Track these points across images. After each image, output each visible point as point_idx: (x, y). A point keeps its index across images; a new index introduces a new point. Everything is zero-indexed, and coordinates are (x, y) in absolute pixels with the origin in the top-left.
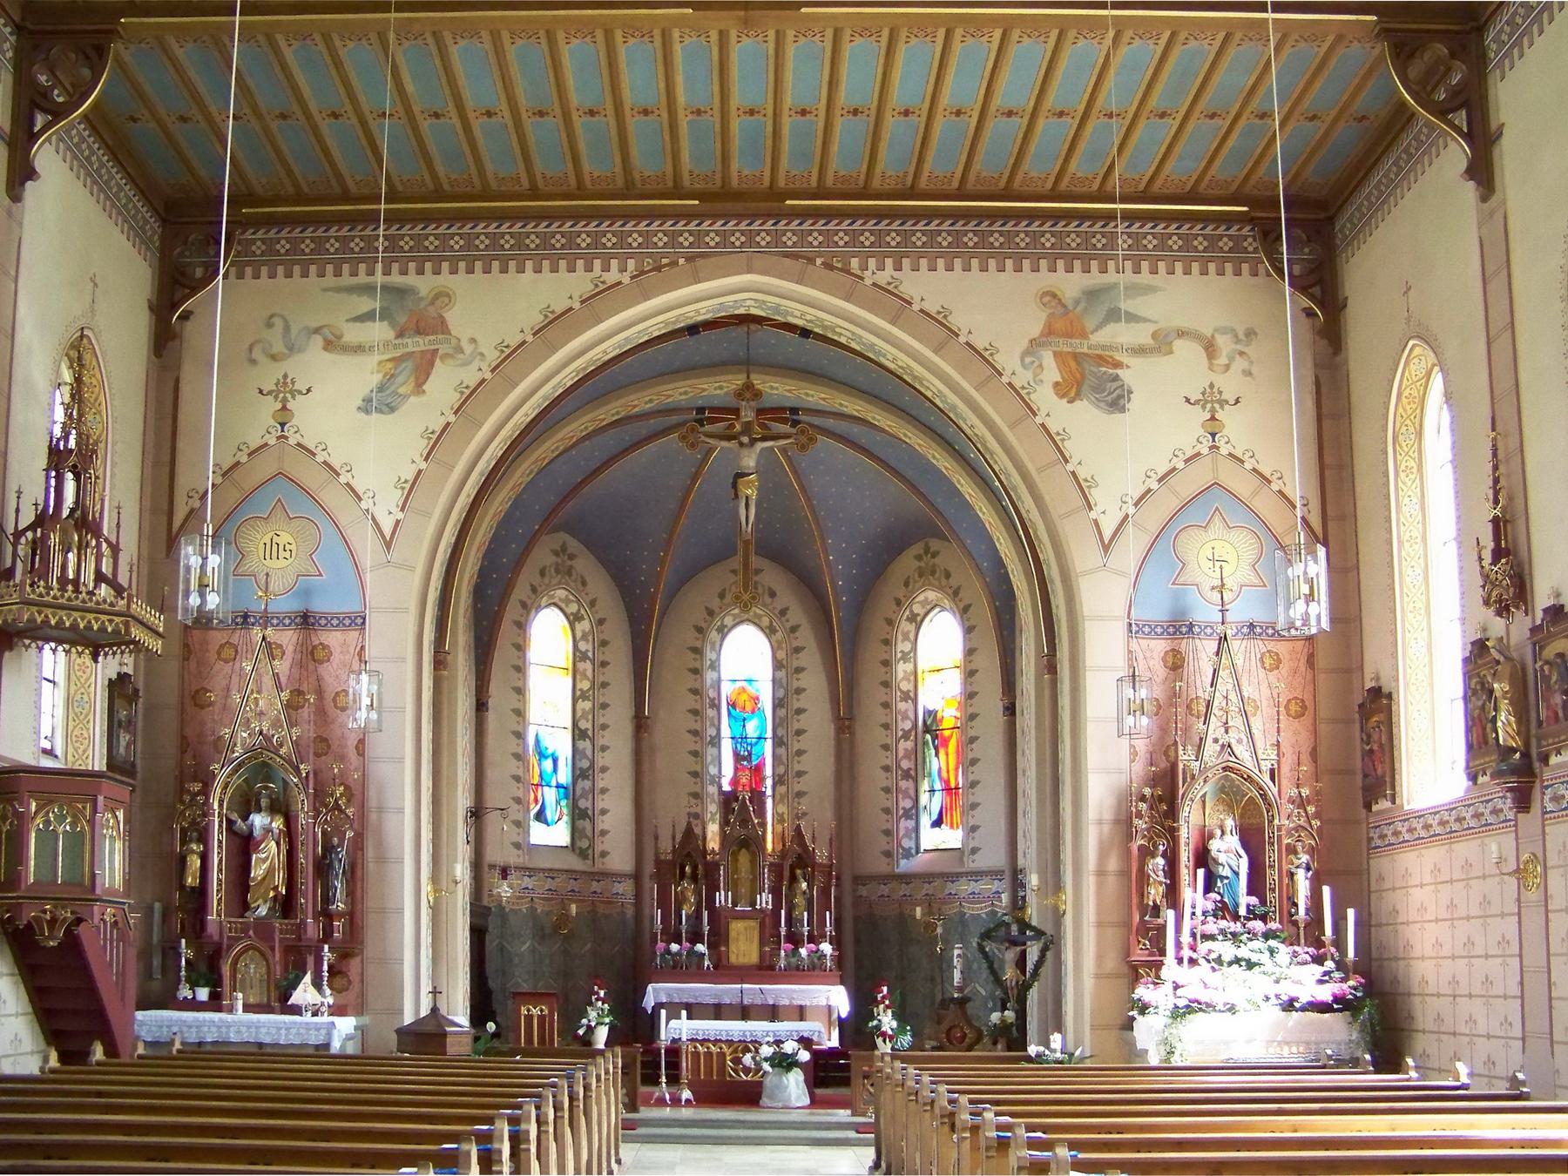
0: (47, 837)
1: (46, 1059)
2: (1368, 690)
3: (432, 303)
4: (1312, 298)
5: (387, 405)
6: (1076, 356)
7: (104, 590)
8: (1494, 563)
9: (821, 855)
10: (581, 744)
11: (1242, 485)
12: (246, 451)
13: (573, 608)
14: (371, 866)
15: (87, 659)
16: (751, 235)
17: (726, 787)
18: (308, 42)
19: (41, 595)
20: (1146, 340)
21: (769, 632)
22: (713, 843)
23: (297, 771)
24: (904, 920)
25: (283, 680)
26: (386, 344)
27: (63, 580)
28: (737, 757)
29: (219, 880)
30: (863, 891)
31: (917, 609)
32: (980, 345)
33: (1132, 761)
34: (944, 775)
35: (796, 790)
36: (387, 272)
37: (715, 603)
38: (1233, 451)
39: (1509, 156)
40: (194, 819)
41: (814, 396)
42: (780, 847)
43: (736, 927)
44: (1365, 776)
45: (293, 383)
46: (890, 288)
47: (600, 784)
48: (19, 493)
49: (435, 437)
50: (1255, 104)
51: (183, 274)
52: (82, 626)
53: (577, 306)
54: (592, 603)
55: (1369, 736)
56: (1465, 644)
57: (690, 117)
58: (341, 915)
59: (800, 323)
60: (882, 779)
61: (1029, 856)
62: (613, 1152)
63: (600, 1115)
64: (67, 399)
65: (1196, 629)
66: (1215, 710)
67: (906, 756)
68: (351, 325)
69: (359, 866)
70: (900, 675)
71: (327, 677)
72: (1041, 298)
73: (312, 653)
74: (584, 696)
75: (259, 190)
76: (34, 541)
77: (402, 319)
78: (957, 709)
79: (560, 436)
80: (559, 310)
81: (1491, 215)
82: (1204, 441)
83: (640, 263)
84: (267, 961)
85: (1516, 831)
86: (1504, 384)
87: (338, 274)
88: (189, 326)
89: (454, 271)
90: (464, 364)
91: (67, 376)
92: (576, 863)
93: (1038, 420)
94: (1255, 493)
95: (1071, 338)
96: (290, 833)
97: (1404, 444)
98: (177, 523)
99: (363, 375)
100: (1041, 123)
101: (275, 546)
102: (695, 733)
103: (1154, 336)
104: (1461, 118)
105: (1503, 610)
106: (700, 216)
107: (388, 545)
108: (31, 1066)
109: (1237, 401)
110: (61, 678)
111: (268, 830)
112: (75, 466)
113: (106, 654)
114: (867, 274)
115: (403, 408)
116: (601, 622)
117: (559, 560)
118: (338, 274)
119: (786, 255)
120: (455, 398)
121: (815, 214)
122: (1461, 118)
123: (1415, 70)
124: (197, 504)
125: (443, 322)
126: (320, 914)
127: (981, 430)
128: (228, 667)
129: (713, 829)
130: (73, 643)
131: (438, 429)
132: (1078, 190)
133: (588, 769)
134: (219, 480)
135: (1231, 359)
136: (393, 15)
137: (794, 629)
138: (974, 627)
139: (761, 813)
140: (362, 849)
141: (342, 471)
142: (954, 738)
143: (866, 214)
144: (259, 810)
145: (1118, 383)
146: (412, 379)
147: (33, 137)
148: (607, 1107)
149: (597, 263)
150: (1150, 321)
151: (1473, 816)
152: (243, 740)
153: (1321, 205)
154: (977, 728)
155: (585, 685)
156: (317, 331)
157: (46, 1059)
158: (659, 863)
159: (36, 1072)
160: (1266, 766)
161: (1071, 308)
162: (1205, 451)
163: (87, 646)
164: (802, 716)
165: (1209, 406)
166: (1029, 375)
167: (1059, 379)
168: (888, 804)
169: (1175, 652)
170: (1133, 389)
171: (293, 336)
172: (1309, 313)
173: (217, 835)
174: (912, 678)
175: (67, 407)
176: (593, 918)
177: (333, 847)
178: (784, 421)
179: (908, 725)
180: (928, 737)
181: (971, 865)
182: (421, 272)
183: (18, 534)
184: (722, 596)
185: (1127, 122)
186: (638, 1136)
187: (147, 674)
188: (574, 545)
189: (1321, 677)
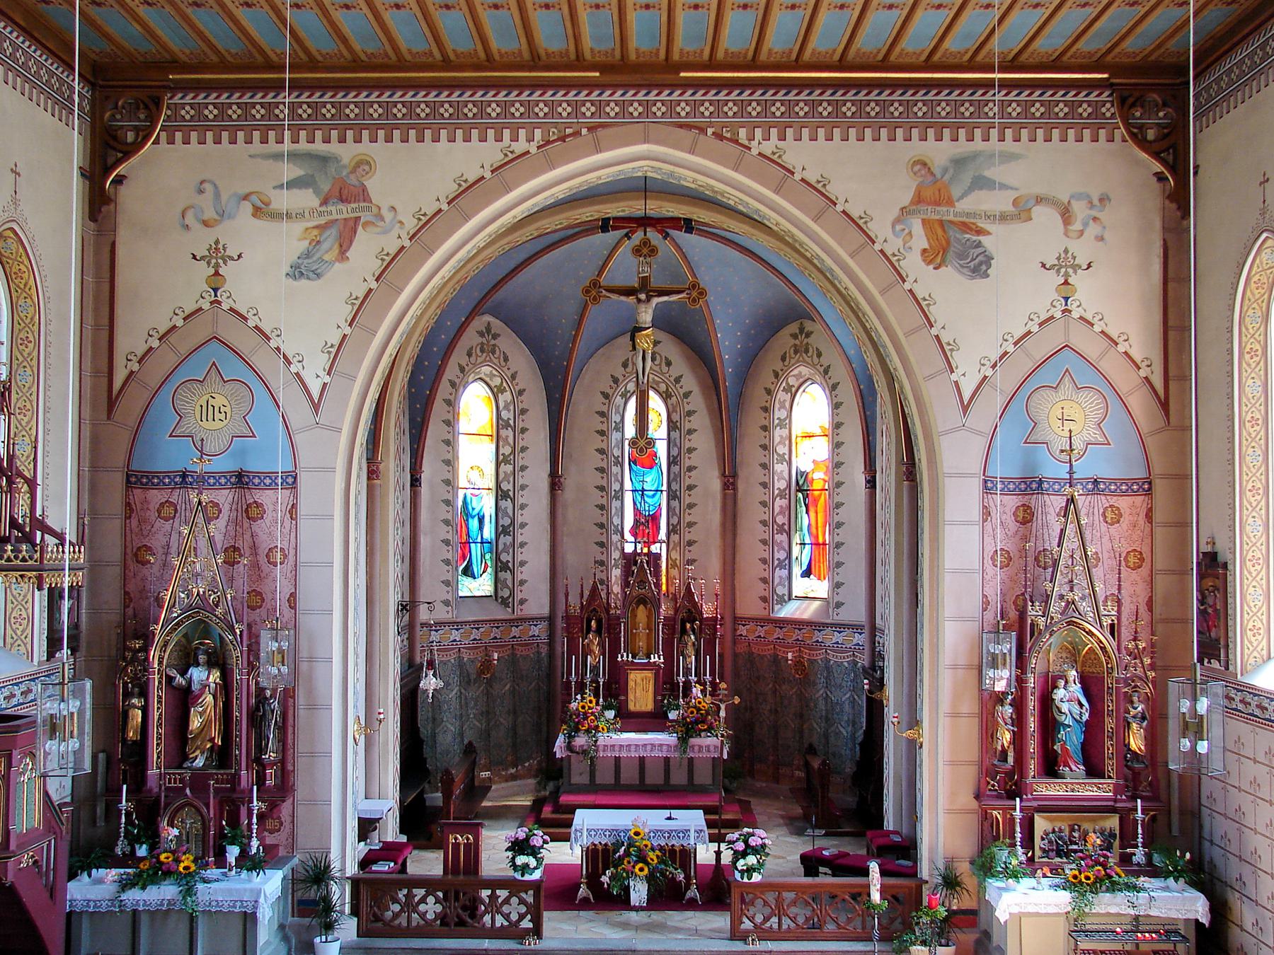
3: (354, 171)
4: (1163, 162)
6: (941, 223)
9: (708, 610)
10: (503, 504)
11: (1090, 346)
12: (182, 315)
13: (497, 381)
14: (302, 713)
16: (647, 105)
20: (1009, 208)
24: (776, 661)
26: (312, 211)
30: (742, 630)
31: (792, 381)
32: (855, 214)
33: (984, 610)
34: (814, 530)
35: (687, 539)
37: (619, 371)
40: (136, 674)
43: (635, 677)
45: (225, 249)
46: (775, 157)
47: (520, 539)
49: (358, 302)
51: (115, 138)
54: (513, 377)
57: (589, 10)
58: (272, 764)
65: (1045, 485)
67: (781, 513)
70: (777, 439)
71: (260, 534)
72: (913, 165)
73: (247, 511)
74: (506, 461)
77: (325, 187)
78: (825, 473)
80: (471, 179)
83: (546, 133)
87: (264, 141)
88: (123, 190)
89: (374, 140)
90: (385, 232)
92: (500, 613)
93: (907, 286)
94: (1103, 355)
95: (939, 205)
97: (1250, 327)
98: (117, 384)
101: (210, 408)
102: (602, 488)
103: (1015, 202)
106: (603, 87)
107: (316, 407)
109: (1089, 266)
114: (754, 144)
116: (521, 393)
118: (264, 141)
119: (681, 126)
120: (377, 266)
121: (707, 85)
125: (364, 189)
126: (253, 761)
128: (168, 525)
131: (361, 295)
135: (1086, 225)
137: (687, 395)
139: (657, 574)
140: (293, 697)
142: (823, 497)
143: (753, 85)
144: (198, 665)
145: (980, 250)
146: (336, 246)
150: (1012, 188)
155: (507, 450)
158: (567, 617)
160: (1106, 622)
161: (939, 176)
162: (1058, 315)
164: (693, 473)
165: (1063, 270)
166: (899, 242)
167: (927, 246)
168: (765, 555)
169: (1026, 507)
170: (995, 255)
171: (223, 203)
172: (1160, 177)
174: (787, 442)
176: (512, 661)
177: (266, 698)
179: (781, 484)
180: (800, 495)
182: (342, 140)
188: (497, 324)
189: (1159, 532)
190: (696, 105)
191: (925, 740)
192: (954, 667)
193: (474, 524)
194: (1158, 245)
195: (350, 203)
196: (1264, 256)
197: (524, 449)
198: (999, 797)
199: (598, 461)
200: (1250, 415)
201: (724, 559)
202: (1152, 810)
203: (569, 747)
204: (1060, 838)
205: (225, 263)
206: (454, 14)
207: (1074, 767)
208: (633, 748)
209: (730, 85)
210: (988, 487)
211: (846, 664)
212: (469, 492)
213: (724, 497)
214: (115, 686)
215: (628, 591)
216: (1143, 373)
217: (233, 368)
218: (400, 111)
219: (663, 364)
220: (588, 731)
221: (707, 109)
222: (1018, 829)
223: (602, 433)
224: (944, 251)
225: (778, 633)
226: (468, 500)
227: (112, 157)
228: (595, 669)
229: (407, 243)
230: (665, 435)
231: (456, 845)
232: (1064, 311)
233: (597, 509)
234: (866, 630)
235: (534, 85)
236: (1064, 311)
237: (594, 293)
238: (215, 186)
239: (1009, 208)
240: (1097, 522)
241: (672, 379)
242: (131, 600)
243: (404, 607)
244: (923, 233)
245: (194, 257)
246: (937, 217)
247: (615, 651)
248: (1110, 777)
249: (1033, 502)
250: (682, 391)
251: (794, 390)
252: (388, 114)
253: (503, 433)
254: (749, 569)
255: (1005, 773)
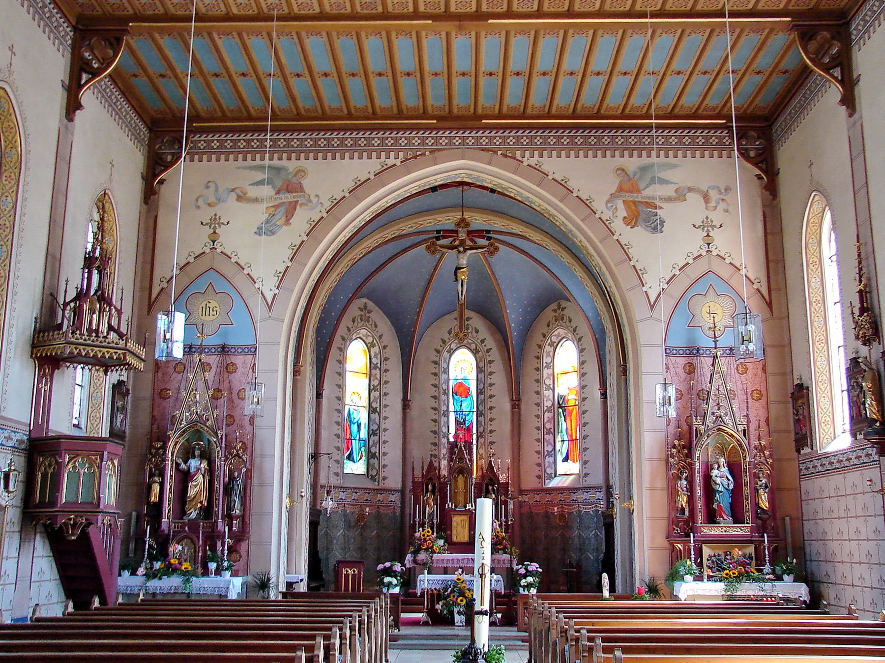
0: (75, 474)
1: (66, 607)
2: (796, 385)
4: (760, 169)
5: (271, 231)
6: (634, 202)
7: (113, 335)
8: (860, 316)
9: (502, 479)
10: (373, 416)
11: (724, 271)
13: (370, 339)
15: (101, 374)
16: (464, 139)
17: (452, 440)
18: (230, 36)
19: (77, 339)
20: (673, 194)
21: (475, 352)
22: (444, 472)
23: (216, 434)
24: (547, 515)
25: (210, 383)
26: (271, 198)
27: (90, 330)
28: (458, 422)
29: (170, 498)
31: (554, 339)
32: (584, 198)
34: (570, 432)
36: (271, 159)
37: (446, 337)
38: (719, 254)
39: (863, 91)
40: (157, 463)
41: (497, 223)
42: (480, 473)
44: (796, 434)
45: (220, 219)
47: (383, 438)
48: (67, 281)
49: (296, 248)
50: (725, 68)
51: (161, 159)
52: (99, 356)
53: (372, 177)
54: (380, 337)
55: (797, 411)
56: (846, 360)
57: (432, 77)
58: (237, 517)
59: (490, 186)
60: (536, 434)
61: (615, 480)
62: (384, 655)
63: (376, 633)
64: (96, 230)
65: (701, 352)
66: (712, 396)
67: (548, 421)
68: (251, 187)
69: (249, 488)
70: (545, 376)
75: (203, 114)
76: (75, 307)
77: (279, 184)
79: (363, 246)
81: (855, 123)
82: (703, 247)
84: (194, 544)
85: (880, 467)
86: (863, 216)
87: (245, 159)
88: (163, 187)
89: (307, 159)
90: (313, 209)
91: (97, 217)
92: (370, 485)
94: (732, 276)
96: (211, 470)
98: (154, 296)
99: (258, 214)
100: (615, 79)
101: (208, 309)
102: (435, 409)
103: (676, 191)
104: (837, 72)
105: (867, 342)
106: (438, 129)
107: (270, 308)
108: (57, 611)
110: (86, 383)
111: (198, 469)
112: (99, 267)
113: (112, 371)
114: (525, 159)
115: (279, 233)
116: (385, 347)
117: (363, 313)
118: (245, 159)
119: (483, 150)
120: (307, 228)
122: (837, 72)
123: (812, 46)
124: (165, 285)
127: (586, 243)
129: (444, 463)
130: (94, 365)
132: (635, 113)
133: (377, 430)
134: (178, 272)
136: (275, 23)
137: (488, 351)
138: (585, 349)
139: (470, 453)
141: (245, 267)
144: (194, 457)
147: (81, 87)
148: (381, 627)
149: (383, 154)
151: (856, 458)
152: (185, 417)
153: (766, 119)
154: (587, 406)
155: (376, 383)
156: (233, 190)
157: (66, 607)
159: (60, 615)
160: (741, 428)
161: (632, 176)
162: (704, 253)
163: (102, 366)
165: (706, 229)
166: (610, 213)
168: (539, 449)
169: (690, 364)
172: (759, 177)
173: (169, 472)
174: (552, 377)
175: (95, 234)
176: (378, 517)
178: (483, 237)
179: (549, 404)
180: (560, 410)
181: (584, 483)
183: (66, 304)
184: (450, 333)
185: (660, 77)
186: (399, 645)
187: (134, 382)
188: (370, 304)
189: (770, 379)
190: (491, 139)
191: (635, 508)
192: (651, 460)
193: (354, 428)
194: (760, 217)
195: (292, 193)
196: (814, 207)
197: (386, 382)
198: (681, 536)
199: (433, 391)
200: (815, 298)
201: (513, 454)
202: (774, 543)
203: (415, 561)
204: (718, 560)
205: (220, 227)
206: (357, 79)
207: (725, 518)
208: (456, 561)
209: (511, 127)
210: (669, 352)
211: (591, 513)
212: (352, 408)
213: (513, 414)
214: (145, 470)
215: (452, 464)
216: (755, 286)
217: (221, 286)
218: (323, 143)
219: (474, 332)
220: (427, 550)
221: (497, 141)
222: (692, 552)
223: (435, 374)
224: (636, 218)
225: (548, 497)
226: (351, 413)
227: (159, 168)
228: (431, 515)
229: (325, 215)
230: (475, 377)
231: (347, 575)
232: (707, 251)
233: (432, 434)
234: (604, 489)
235: (399, 128)
236: (707, 251)
237: (432, 249)
238: (216, 185)
239: (673, 194)
240: (733, 373)
241: (479, 341)
242: (156, 420)
243: (313, 457)
244: (623, 207)
245: (202, 223)
246: (632, 199)
247: (444, 501)
248: (747, 523)
249: (694, 361)
250: (485, 348)
251: (555, 344)
252: (316, 144)
253: (373, 372)
254: (529, 458)
255: (684, 521)
